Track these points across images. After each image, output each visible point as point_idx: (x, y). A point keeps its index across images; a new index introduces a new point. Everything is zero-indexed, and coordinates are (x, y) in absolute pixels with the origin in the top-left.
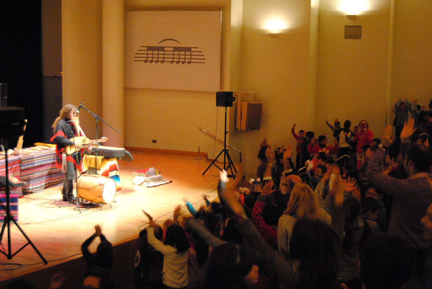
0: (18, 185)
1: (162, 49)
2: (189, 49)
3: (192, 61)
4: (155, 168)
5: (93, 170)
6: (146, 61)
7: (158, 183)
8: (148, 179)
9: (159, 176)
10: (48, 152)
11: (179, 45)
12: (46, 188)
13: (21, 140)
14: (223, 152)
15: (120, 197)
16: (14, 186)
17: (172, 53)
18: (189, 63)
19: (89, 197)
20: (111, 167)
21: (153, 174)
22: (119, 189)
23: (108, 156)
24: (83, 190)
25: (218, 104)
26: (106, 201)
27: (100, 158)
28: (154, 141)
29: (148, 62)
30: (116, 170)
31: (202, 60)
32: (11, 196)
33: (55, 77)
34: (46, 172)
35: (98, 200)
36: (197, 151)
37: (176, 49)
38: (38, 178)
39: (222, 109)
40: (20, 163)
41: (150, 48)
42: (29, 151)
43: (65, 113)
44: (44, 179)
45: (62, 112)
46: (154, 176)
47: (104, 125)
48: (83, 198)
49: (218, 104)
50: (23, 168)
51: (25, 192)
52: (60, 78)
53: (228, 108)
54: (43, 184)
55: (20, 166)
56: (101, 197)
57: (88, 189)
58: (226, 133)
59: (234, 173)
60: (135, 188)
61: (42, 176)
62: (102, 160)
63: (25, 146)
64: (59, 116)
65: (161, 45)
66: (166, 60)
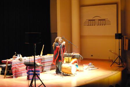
0: (40, 66)
1: (94, 20)
2: (104, 20)
3: (106, 24)
4: (92, 63)
5: (68, 62)
6: (88, 25)
7: (94, 69)
8: (89, 67)
9: (93, 66)
10: (50, 57)
11: (101, 19)
12: (51, 70)
13: (42, 53)
14: (119, 57)
15: (78, 72)
16: (38, 66)
17: (98, 21)
18: (105, 25)
19: (66, 72)
20: (74, 62)
21: (91, 65)
22: (78, 70)
23: (73, 57)
24: (64, 69)
25: (116, 38)
26: (73, 73)
27: (70, 58)
28: (92, 56)
29: (89, 26)
30: (77, 63)
31: (109, 24)
32: (36, 70)
33: (55, 33)
34: (51, 64)
35: (70, 72)
36: (108, 59)
37: (99, 20)
38: (48, 66)
39: (118, 40)
40: (41, 60)
41: (89, 20)
42: (45, 56)
43: (57, 40)
44: (50, 66)
45: (56, 40)
46: (91, 66)
47: (73, 45)
48: (64, 72)
49: (116, 38)
50: (42, 62)
51: (43, 71)
52: (57, 33)
53: (120, 40)
54: (50, 68)
55: (41, 61)
56: (71, 71)
57: (66, 69)
58: (119, 49)
59: (123, 66)
60: (84, 70)
61: (49, 65)
62: (71, 59)
63: (43, 55)
64: (55, 42)
65: (94, 19)
66: (96, 24)
